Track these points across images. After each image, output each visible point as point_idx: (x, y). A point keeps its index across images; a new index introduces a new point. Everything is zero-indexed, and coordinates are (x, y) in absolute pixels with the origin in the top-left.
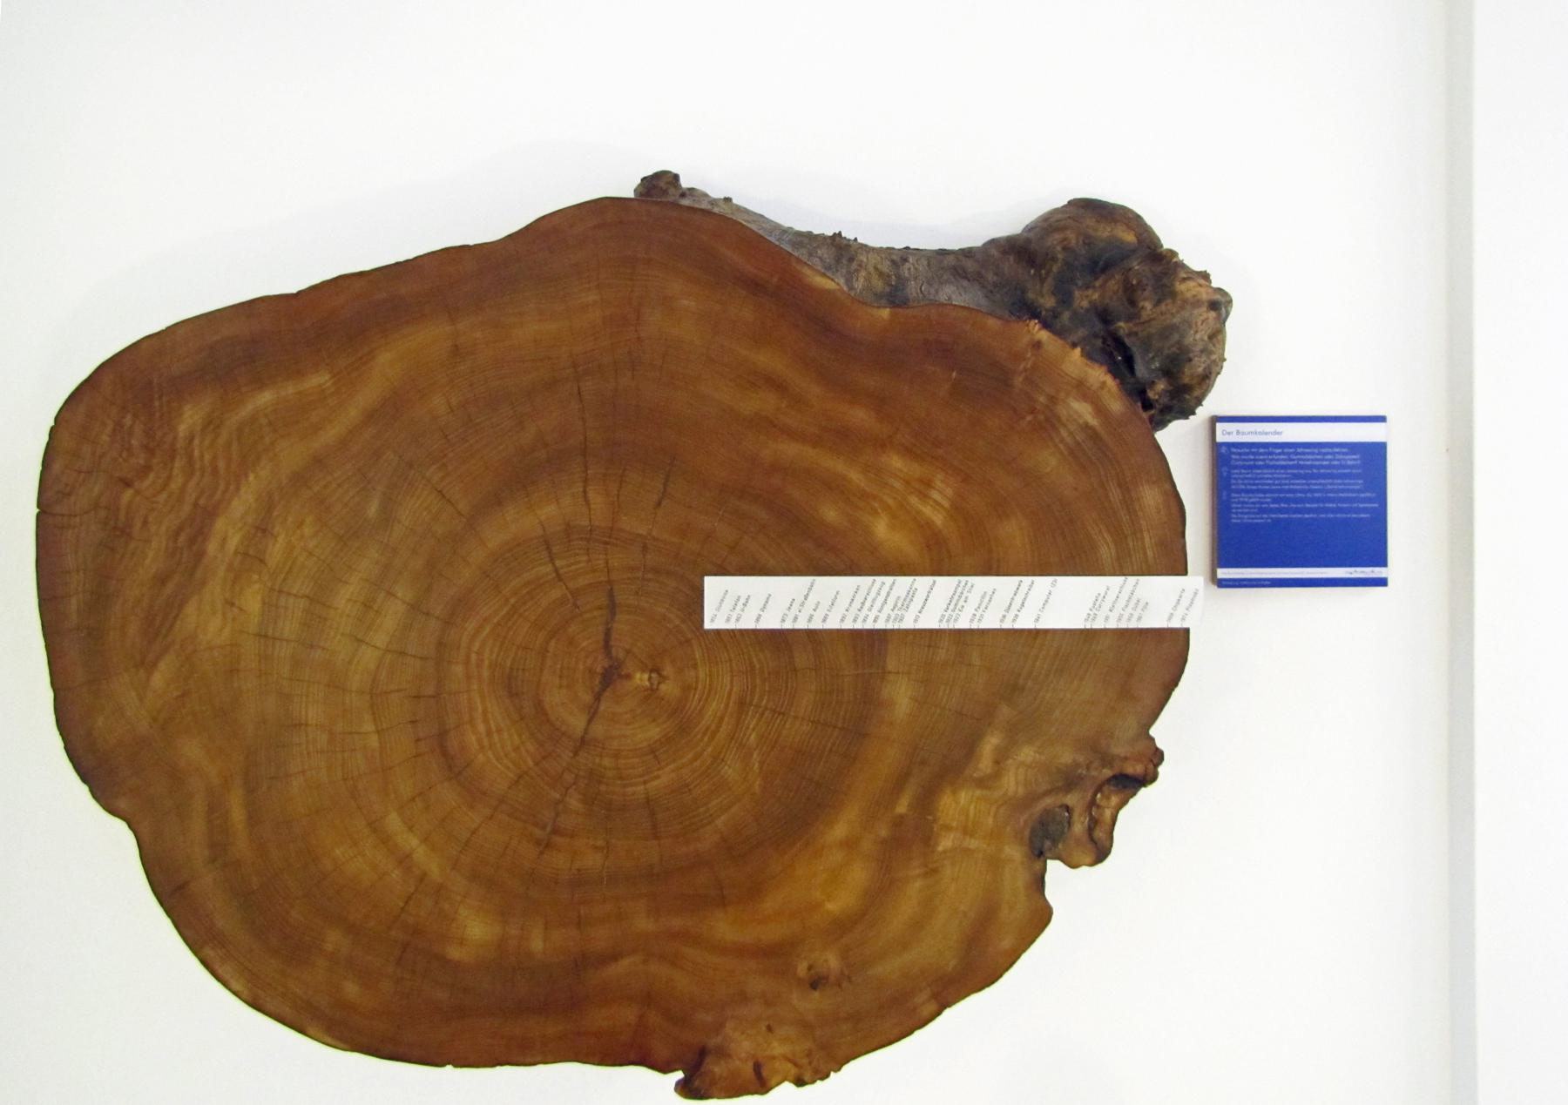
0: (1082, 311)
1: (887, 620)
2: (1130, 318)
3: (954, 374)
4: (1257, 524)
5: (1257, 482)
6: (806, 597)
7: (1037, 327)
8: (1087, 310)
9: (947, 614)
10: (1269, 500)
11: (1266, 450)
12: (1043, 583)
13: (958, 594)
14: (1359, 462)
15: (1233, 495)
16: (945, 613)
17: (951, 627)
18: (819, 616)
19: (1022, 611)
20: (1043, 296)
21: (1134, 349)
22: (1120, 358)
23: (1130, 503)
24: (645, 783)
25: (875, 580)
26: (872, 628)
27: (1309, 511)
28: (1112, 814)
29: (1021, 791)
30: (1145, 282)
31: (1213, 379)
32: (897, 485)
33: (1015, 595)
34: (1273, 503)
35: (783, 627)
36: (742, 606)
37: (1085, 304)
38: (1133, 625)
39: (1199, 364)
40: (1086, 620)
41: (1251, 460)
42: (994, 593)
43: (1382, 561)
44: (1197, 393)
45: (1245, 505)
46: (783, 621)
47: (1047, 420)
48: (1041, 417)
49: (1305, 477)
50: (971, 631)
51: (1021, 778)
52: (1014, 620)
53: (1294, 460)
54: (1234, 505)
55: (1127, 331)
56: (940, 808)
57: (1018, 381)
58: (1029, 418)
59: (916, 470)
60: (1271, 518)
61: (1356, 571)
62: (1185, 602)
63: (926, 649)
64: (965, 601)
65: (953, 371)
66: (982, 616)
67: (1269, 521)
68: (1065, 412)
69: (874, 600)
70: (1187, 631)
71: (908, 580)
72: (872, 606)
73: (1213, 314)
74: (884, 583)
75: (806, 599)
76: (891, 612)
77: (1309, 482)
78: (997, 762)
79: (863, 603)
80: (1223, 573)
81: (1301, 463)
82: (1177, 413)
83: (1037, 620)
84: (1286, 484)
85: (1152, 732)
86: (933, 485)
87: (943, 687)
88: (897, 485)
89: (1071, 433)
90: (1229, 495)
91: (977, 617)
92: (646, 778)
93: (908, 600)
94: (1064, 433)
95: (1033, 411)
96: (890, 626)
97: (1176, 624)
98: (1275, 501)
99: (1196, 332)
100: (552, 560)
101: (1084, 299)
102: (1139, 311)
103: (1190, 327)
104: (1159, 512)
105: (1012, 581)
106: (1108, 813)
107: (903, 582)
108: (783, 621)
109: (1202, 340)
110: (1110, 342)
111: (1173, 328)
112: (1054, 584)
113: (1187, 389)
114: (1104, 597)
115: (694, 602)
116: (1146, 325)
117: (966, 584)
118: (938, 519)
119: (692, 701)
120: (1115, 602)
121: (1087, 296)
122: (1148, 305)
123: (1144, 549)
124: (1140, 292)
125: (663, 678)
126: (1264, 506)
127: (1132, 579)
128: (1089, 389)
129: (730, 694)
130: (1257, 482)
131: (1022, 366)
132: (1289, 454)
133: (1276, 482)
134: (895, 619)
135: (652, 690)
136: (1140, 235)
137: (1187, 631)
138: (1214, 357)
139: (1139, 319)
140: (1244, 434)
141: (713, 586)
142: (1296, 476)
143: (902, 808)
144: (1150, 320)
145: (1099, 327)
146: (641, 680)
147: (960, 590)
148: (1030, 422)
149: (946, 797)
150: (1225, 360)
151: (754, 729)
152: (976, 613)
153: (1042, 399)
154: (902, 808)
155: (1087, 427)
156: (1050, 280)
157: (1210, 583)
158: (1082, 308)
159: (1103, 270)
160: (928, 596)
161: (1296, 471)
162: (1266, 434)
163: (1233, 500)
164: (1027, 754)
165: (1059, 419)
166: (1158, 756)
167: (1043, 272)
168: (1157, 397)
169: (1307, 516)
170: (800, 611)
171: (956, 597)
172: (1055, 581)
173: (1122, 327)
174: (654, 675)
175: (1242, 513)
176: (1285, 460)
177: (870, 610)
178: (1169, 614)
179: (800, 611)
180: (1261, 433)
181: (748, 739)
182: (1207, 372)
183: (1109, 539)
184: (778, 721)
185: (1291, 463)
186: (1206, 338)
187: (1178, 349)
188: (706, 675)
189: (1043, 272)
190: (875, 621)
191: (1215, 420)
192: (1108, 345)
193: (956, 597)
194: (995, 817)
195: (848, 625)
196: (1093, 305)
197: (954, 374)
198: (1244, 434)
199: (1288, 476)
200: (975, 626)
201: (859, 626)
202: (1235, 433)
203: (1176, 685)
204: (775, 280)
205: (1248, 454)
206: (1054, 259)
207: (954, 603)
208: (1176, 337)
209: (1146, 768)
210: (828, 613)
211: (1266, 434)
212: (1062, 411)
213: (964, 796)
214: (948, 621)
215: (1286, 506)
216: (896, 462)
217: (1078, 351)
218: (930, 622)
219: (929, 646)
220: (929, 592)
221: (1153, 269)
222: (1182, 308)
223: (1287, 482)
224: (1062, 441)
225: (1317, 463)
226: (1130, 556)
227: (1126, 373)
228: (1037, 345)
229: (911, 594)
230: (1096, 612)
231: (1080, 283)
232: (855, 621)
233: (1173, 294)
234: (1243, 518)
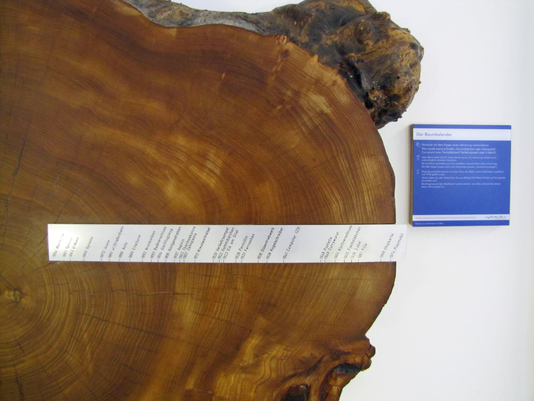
0: (327, 46)
1: (175, 257)
2: (358, 51)
3: (224, 75)
4: (438, 188)
5: (436, 164)
6: (117, 239)
7: (285, 41)
8: (330, 47)
9: (218, 252)
10: (443, 175)
11: (442, 145)
12: (289, 230)
13: (226, 238)
14: (495, 152)
15: (423, 171)
16: (217, 252)
17: (221, 261)
18: (127, 253)
19: (274, 250)
20: (300, 36)
21: (361, 71)
22: (352, 76)
23: (353, 170)
24: (14, 365)
25: (165, 227)
26: (165, 262)
27: (467, 181)
28: (338, 390)
29: (274, 375)
30: (368, 28)
31: (413, 92)
32: (182, 158)
33: (269, 238)
34: (446, 177)
35: (103, 261)
36: (74, 245)
37: (329, 42)
38: (355, 260)
39: (404, 81)
40: (321, 257)
41: (433, 151)
42: (252, 237)
43: (507, 212)
44: (403, 101)
45: (429, 178)
46: (102, 256)
47: (293, 108)
48: (288, 107)
49: (465, 161)
50: (237, 265)
51: (273, 365)
52: (268, 257)
53: (458, 151)
54: (423, 178)
55: (356, 59)
56: (218, 386)
57: (271, 80)
58: (279, 107)
59: (196, 146)
60: (445, 186)
61: (492, 217)
62: (393, 243)
63: (204, 277)
64: (232, 243)
65: (223, 73)
66: (244, 254)
67: (443, 187)
68: (305, 102)
69: (165, 242)
70: (394, 264)
71: (190, 227)
72: (164, 246)
73: (412, 51)
74: (172, 230)
75: (117, 241)
76: (178, 251)
77: (467, 164)
78: (256, 356)
79: (157, 244)
80: (416, 218)
81: (462, 153)
82: (389, 115)
83: (285, 257)
84: (453, 165)
85: (368, 335)
86: (208, 157)
87: (217, 304)
88: (182, 158)
89: (310, 119)
90: (420, 172)
91: (241, 255)
92: (15, 362)
93: (190, 242)
94: (306, 119)
95: (282, 102)
96: (177, 261)
97: (386, 259)
98: (446, 175)
99: (402, 61)
101: (327, 40)
103: (398, 56)
104: (375, 177)
105: (265, 229)
106: (335, 389)
107: (186, 229)
108: (102, 256)
109: (406, 66)
110: (344, 66)
111: (386, 57)
112: (297, 231)
113: (397, 97)
114: (335, 240)
116: (369, 55)
117: (232, 231)
118: (212, 183)
119: (44, 310)
120: (342, 244)
121: (331, 39)
122: (371, 43)
123: (364, 205)
124: (365, 35)
125: (23, 295)
126: (440, 178)
127: (355, 227)
128: (324, 86)
129: (69, 305)
130: (436, 164)
131: (274, 69)
132: (455, 147)
133: (448, 164)
134: (181, 256)
135: (17, 303)
136: (367, 8)
137: (394, 264)
138: (413, 78)
139: (365, 51)
140: (429, 135)
142: (459, 161)
143: (190, 385)
144: (371, 53)
145: (338, 56)
146: (8, 295)
147: (227, 235)
148: (280, 110)
149: (221, 378)
150: (420, 83)
151: (86, 331)
152: (239, 251)
153: (289, 93)
154: (190, 385)
155: (322, 114)
156: (306, 27)
157: (409, 224)
158: (327, 44)
159: (343, 24)
160: (204, 239)
161: (459, 158)
162: (442, 135)
163: (422, 175)
164: (278, 351)
165: (301, 107)
166: (372, 351)
167: (302, 23)
168: (375, 99)
169: (464, 184)
170: (113, 249)
171: (225, 241)
172: (298, 228)
173: (354, 56)
174: (17, 292)
175: (428, 182)
176: (453, 151)
177: (162, 249)
179: (113, 249)
180: (439, 135)
181: (82, 337)
182: (410, 86)
183: (339, 198)
184: (102, 325)
185: (456, 153)
186: (408, 65)
187: (390, 70)
188: (52, 293)
189: (302, 23)
190: (166, 257)
191: (412, 127)
192: (344, 68)
193: (225, 241)
194: (255, 392)
195: (147, 260)
196: (335, 44)
197: (224, 75)
198: (429, 135)
199: (455, 160)
200: (239, 261)
201: (155, 260)
202: (424, 134)
203: (386, 302)
204: (94, 10)
205: (432, 147)
206: (310, 16)
208: (389, 62)
209: (363, 359)
210: (133, 251)
211: (442, 135)
212: (303, 102)
213: (233, 378)
214: (219, 257)
216: (181, 141)
217: (316, 57)
218: (206, 258)
219: (206, 275)
220: (205, 236)
221: (374, 22)
222: (393, 45)
223: (454, 164)
224: (304, 124)
225: (472, 153)
226: (354, 209)
227: (356, 86)
228: (286, 53)
229: (192, 237)
230: (329, 251)
232: (152, 257)
233: (387, 37)
234: (429, 185)
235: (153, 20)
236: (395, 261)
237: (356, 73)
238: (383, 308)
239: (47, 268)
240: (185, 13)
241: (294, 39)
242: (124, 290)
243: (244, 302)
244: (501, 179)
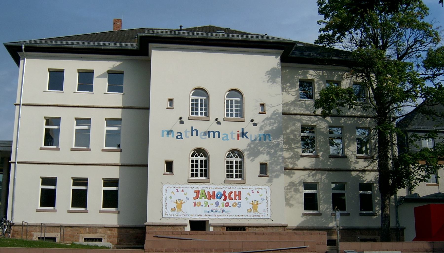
28: (332, 227)
65: (378, 205)
86: (287, 206)
100: (27, 235)
102: (329, 24)
115: (340, 122)
141: (211, 231)
146: (295, 80)
178: (284, 116)
207: (93, 244)
211: (334, 247)
215: (406, 144)
231: (347, 34)
235: (300, 117)
236: (210, 136)
237: (423, 137)
238: (415, 236)
239: (352, 97)
240: (270, 130)
241: (428, 11)
242: (27, 237)
243: (266, 230)
244: (336, 35)
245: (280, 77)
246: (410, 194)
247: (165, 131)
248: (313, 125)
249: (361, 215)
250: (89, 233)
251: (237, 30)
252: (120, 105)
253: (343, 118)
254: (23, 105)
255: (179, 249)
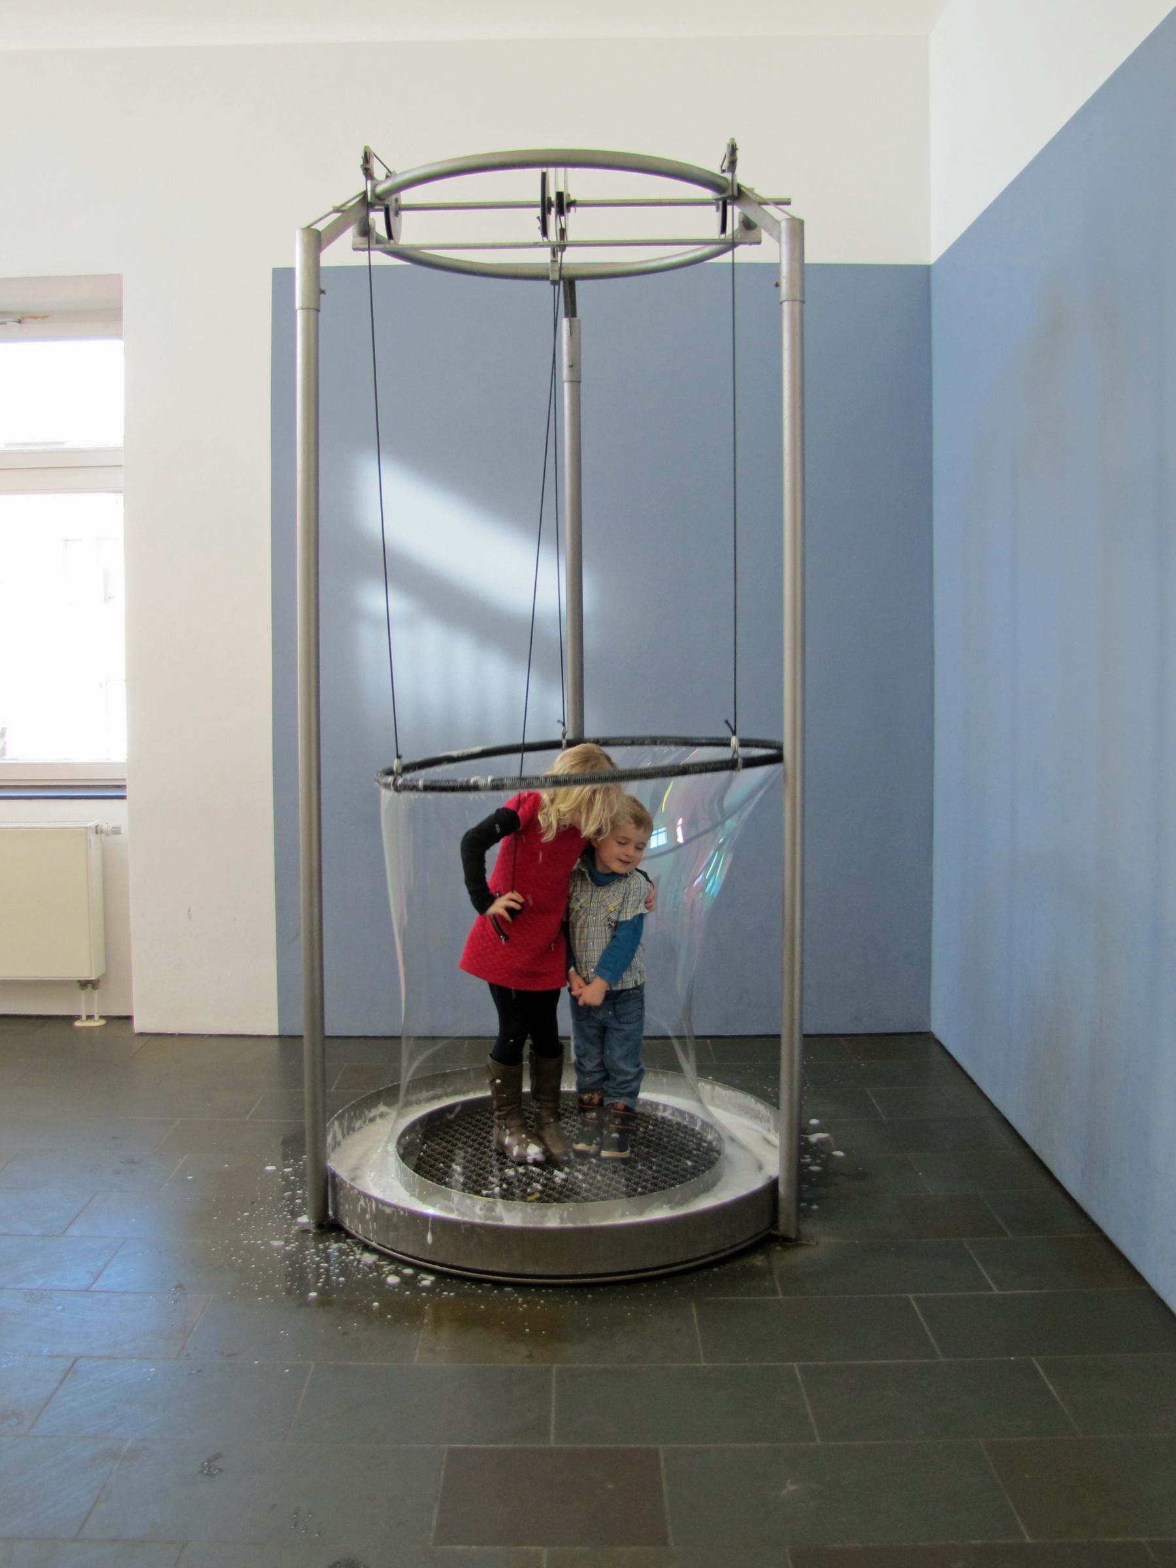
115: (808, 1122)
245: (451, 1192)
246: (113, 791)
247: (783, 220)
248: (539, 1548)
249: (125, 780)
250: (447, 1095)
251: (1010, 1121)
252: (735, 262)
253: (314, 1223)
254: (544, 176)
255: (497, 1113)
